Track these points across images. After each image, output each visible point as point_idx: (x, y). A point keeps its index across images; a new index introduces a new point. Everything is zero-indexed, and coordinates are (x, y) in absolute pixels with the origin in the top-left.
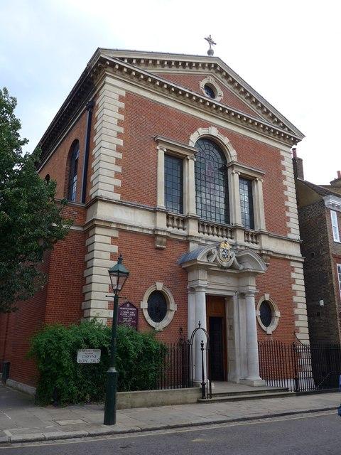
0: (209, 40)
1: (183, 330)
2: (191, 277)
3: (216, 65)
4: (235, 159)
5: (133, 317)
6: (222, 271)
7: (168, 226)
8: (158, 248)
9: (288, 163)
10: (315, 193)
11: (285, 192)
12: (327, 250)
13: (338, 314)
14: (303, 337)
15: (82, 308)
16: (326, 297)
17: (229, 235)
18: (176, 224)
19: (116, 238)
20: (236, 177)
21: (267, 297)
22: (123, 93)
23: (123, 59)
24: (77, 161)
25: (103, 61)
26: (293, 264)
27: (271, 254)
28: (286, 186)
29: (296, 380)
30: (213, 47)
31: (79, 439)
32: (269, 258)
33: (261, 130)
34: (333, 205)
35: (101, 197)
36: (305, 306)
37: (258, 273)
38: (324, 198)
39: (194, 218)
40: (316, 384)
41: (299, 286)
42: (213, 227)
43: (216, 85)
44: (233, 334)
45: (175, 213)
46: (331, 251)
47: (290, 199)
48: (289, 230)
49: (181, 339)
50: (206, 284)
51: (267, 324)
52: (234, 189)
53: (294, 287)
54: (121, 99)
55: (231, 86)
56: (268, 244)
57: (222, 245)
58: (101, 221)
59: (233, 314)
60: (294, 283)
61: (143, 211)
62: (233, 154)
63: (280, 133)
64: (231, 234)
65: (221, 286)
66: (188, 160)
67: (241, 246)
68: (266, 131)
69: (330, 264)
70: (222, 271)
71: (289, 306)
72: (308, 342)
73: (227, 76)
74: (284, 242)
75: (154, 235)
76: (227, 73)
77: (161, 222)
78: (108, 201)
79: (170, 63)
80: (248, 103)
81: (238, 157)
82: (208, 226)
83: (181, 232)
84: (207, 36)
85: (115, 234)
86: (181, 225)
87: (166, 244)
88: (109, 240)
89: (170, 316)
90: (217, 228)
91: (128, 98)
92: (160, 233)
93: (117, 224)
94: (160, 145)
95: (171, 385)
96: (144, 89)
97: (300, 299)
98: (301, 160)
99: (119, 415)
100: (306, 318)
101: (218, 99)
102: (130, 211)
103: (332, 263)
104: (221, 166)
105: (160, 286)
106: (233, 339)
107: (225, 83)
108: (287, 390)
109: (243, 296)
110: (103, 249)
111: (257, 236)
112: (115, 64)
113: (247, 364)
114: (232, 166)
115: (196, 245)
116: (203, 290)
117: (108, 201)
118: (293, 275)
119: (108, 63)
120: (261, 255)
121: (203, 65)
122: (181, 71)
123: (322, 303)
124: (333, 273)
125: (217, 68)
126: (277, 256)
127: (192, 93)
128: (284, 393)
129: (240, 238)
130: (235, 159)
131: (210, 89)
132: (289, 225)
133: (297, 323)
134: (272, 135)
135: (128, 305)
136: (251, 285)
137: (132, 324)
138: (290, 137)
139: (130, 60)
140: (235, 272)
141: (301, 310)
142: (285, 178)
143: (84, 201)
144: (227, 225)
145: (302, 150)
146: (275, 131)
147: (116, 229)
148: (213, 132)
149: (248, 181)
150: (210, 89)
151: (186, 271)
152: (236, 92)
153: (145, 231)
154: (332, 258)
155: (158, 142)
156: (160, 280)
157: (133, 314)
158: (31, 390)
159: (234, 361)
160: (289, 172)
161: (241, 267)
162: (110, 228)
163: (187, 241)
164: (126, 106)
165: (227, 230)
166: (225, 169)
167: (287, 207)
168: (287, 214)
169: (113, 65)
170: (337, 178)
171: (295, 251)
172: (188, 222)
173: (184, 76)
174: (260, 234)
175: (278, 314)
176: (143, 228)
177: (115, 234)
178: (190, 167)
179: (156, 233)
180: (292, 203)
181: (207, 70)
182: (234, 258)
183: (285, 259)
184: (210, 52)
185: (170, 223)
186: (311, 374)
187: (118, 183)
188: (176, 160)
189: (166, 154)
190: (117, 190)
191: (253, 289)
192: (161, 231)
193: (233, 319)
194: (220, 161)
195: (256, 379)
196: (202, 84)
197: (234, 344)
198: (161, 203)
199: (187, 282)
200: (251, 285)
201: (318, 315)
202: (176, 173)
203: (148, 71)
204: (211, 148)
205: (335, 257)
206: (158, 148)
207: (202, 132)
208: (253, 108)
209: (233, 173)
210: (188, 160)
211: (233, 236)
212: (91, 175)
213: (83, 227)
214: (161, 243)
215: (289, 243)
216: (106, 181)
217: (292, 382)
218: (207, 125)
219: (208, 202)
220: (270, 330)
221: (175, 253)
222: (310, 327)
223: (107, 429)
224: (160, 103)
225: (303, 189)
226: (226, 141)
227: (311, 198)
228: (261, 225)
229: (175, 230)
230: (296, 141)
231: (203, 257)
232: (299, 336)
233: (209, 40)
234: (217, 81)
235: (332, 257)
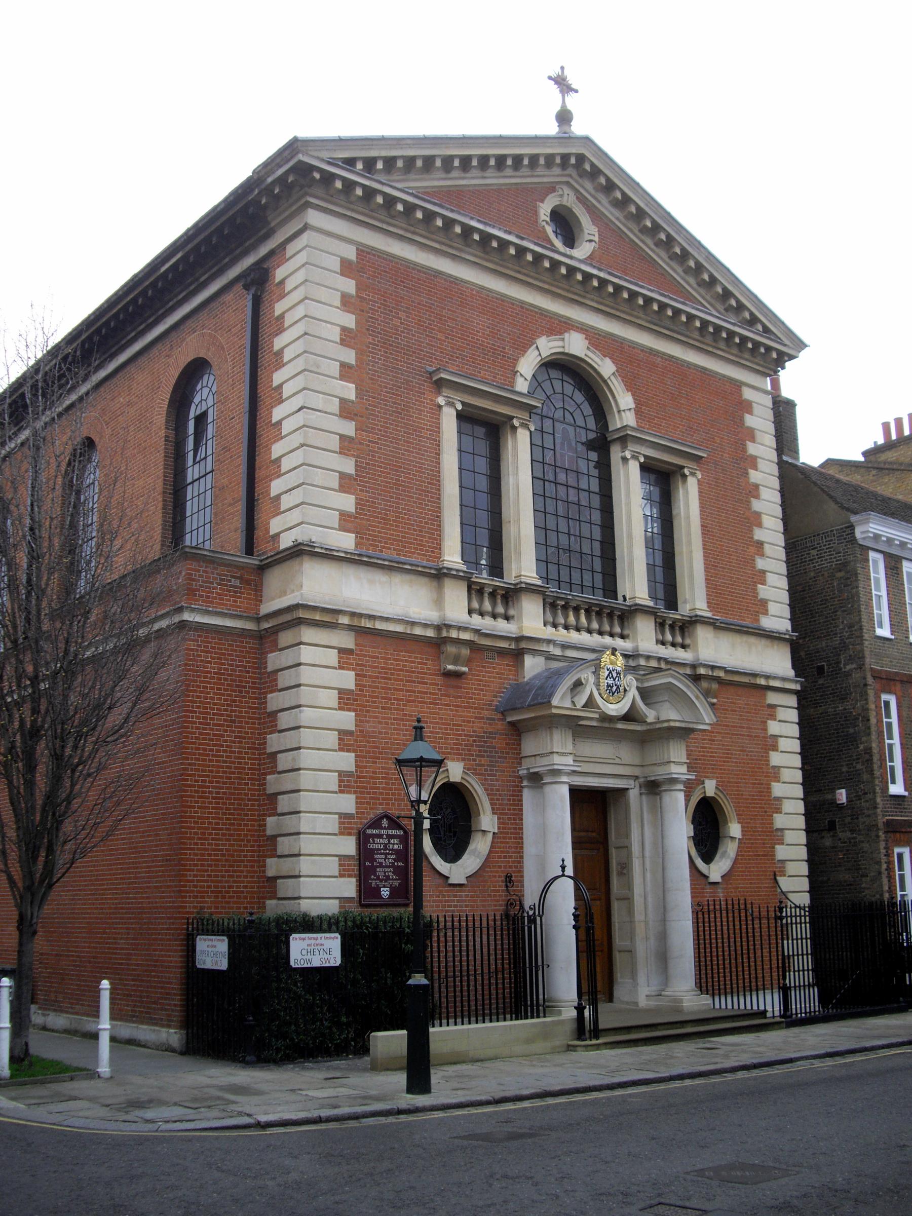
0: (562, 83)
1: (512, 880)
2: (530, 745)
3: (581, 158)
4: (629, 419)
5: (397, 852)
6: (606, 728)
7: (470, 612)
8: (448, 674)
9: (760, 421)
10: (832, 505)
11: (747, 417)
12: (859, 658)
13: (881, 825)
14: (796, 886)
15: (269, 832)
16: (848, 781)
17: (617, 630)
18: (487, 606)
19: (349, 652)
20: (634, 468)
21: (710, 788)
22: (351, 253)
23: (350, 162)
24: (201, 419)
25: (304, 170)
26: (773, 698)
27: (721, 674)
28: (756, 486)
29: (785, 991)
30: (572, 102)
31: (383, 1118)
32: (715, 686)
33: (696, 335)
34: (877, 537)
35: (311, 544)
36: (800, 807)
37: (693, 730)
38: (853, 518)
39: (531, 589)
40: (823, 1000)
41: (787, 757)
42: (576, 610)
43: (580, 212)
44: (629, 886)
45: (484, 577)
46: (867, 660)
47: (767, 521)
48: (762, 606)
49: (509, 904)
50: (567, 761)
51: (708, 858)
52: (629, 504)
53: (775, 759)
54: (347, 268)
55: (617, 213)
56: (714, 649)
57: (606, 658)
58: (315, 608)
59: (628, 835)
60: (775, 748)
61: (408, 577)
62: (624, 407)
63: (744, 339)
64: (622, 627)
65: (607, 765)
66: (514, 428)
67: (648, 658)
68: (710, 337)
69: (864, 696)
70: (606, 728)
71: (764, 807)
72: (804, 899)
73: (610, 187)
74: (752, 640)
75: (438, 641)
76: (608, 179)
77: (455, 606)
78: (328, 556)
79: (466, 161)
80: (660, 258)
81: (638, 412)
82: (565, 608)
83: (502, 627)
84: (555, 71)
85: (347, 641)
86: (500, 609)
87: (468, 662)
88: (332, 657)
89: (479, 848)
90: (588, 612)
91: (364, 266)
92: (454, 634)
93: (353, 615)
94: (446, 392)
95: (484, 1015)
96: (401, 238)
97: (789, 789)
98: (790, 405)
99: (436, 1077)
100: (802, 838)
101: (582, 251)
102: (380, 577)
103: (871, 693)
104: (592, 436)
105: (455, 771)
106: (628, 899)
107: (604, 205)
108: (763, 1014)
109: (653, 788)
110: (317, 684)
111: (682, 629)
112: (333, 176)
113: (663, 958)
114: (624, 440)
115: (540, 660)
116: (565, 779)
117: (328, 556)
118: (774, 728)
119: (317, 176)
120: (696, 678)
121: (550, 159)
122: (493, 179)
123: (842, 796)
124: (873, 721)
125: (579, 164)
126: (736, 678)
127: (525, 244)
128: (756, 1022)
129: (645, 637)
130: (629, 419)
131: (565, 225)
132: (763, 591)
133: (779, 821)
134: (722, 345)
135: (385, 822)
136: (676, 762)
137: (396, 870)
138: (769, 349)
139: (370, 163)
140: (633, 731)
141: (791, 818)
142: (753, 462)
143: (249, 549)
144: (609, 602)
145: (792, 380)
146: (732, 334)
147: (350, 628)
148: (576, 345)
149: (662, 478)
150: (565, 225)
151: (517, 730)
152: (631, 232)
153: (418, 631)
154: (870, 680)
155: (440, 384)
156: (459, 755)
157: (396, 844)
158: (173, 1036)
159: (630, 952)
160: (763, 448)
161: (651, 715)
162: (332, 626)
163: (518, 649)
164: (358, 289)
165: (610, 616)
166: (602, 444)
167: (760, 544)
168: (760, 564)
169: (328, 178)
170: (881, 441)
171: (777, 663)
172: (519, 600)
173: (499, 191)
174: (696, 622)
175: (735, 829)
176: (413, 624)
177: (347, 641)
178: (519, 451)
179: (444, 634)
180: (771, 532)
181: (557, 171)
182: (633, 693)
183: (750, 686)
184: (564, 117)
185: (475, 605)
186: (810, 977)
187: (348, 502)
188: (486, 430)
189: (460, 416)
190: (346, 521)
191: (679, 771)
192: (459, 628)
193: (627, 848)
194: (591, 423)
195: (685, 993)
196: (545, 210)
197: (630, 911)
198: (452, 555)
199: (519, 759)
200: (676, 762)
201: (832, 826)
202: (482, 465)
203: (399, 185)
204: (569, 389)
205: (877, 676)
206: (441, 401)
207: (547, 346)
208: (675, 272)
209: (625, 460)
210: (514, 428)
211: (626, 632)
212: (270, 479)
213: (258, 620)
214: (456, 660)
215: (764, 642)
216: (311, 497)
217: (776, 996)
218: (560, 327)
219: (564, 539)
220: (716, 870)
221: (491, 682)
222: (811, 861)
223: (421, 1100)
224: (441, 273)
225: (797, 482)
226: (606, 368)
227: (822, 506)
228: (695, 598)
229: (485, 623)
230: (782, 359)
231: (562, 698)
232: (785, 883)
233: (562, 83)
234: (581, 199)
235: (870, 680)
